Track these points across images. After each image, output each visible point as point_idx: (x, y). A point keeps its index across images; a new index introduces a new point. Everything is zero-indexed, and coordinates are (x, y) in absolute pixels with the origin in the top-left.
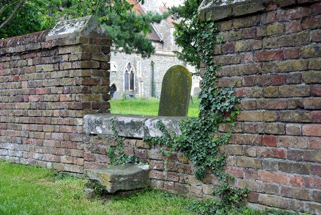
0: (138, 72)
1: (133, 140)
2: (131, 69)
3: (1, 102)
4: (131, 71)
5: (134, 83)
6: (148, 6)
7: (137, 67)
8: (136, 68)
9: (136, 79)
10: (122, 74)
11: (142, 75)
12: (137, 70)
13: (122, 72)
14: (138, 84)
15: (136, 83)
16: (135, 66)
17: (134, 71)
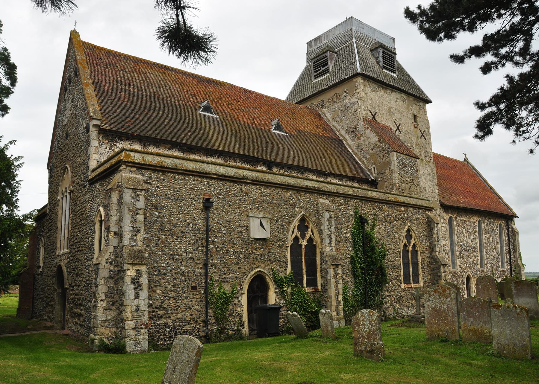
0: (327, 241)
1: (330, 185)
2: (309, 234)
3: (538, 381)
4: (308, 237)
5: (318, 269)
6: (342, 121)
7: (325, 227)
8: (320, 232)
9: (322, 261)
10: (283, 246)
11: (338, 249)
12: (325, 236)
13: (284, 242)
14: (327, 274)
15: (322, 269)
16: (318, 225)
17: (316, 238)
